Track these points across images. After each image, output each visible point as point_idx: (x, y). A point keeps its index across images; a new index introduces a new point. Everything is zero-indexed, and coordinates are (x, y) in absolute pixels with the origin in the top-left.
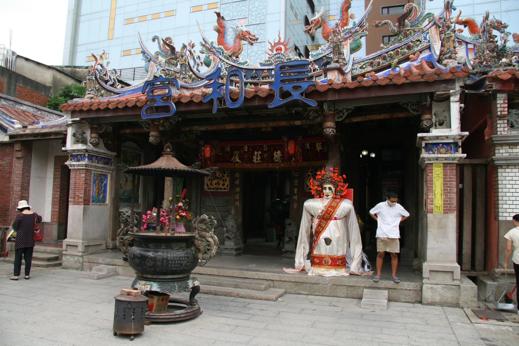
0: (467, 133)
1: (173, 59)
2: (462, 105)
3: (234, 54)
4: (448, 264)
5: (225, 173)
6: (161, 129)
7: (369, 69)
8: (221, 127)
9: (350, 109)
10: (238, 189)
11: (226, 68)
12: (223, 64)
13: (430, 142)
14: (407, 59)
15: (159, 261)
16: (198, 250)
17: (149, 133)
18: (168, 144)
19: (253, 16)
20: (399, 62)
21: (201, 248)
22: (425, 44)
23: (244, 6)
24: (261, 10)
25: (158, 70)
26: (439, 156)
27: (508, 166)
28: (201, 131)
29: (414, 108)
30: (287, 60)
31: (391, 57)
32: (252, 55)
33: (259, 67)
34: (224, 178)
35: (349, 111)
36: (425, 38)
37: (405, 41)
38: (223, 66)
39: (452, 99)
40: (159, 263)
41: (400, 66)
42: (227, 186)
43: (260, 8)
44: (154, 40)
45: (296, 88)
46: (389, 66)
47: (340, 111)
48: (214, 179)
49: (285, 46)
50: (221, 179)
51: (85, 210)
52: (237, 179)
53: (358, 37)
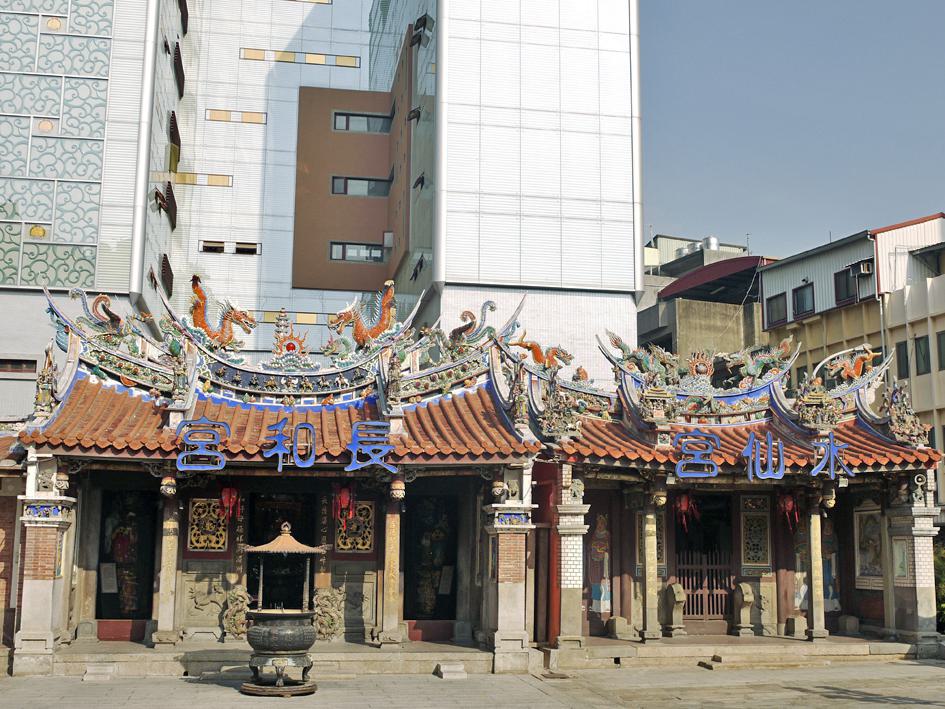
0: (536, 506)
1: (115, 335)
2: (535, 483)
4: (517, 632)
5: (220, 525)
7: (415, 391)
11: (209, 365)
12: (203, 356)
14: (462, 383)
17: (161, 479)
19: (72, 117)
22: (484, 368)
23: (50, 89)
24: (92, 109)
25: (85, 349)
26: (512, 526)
36: (484, 360)
38: (205, 362)
39: (525, 471)
42: (224, 544)
45: (374, 451)
46: (440, 391)
52: (240, 534)
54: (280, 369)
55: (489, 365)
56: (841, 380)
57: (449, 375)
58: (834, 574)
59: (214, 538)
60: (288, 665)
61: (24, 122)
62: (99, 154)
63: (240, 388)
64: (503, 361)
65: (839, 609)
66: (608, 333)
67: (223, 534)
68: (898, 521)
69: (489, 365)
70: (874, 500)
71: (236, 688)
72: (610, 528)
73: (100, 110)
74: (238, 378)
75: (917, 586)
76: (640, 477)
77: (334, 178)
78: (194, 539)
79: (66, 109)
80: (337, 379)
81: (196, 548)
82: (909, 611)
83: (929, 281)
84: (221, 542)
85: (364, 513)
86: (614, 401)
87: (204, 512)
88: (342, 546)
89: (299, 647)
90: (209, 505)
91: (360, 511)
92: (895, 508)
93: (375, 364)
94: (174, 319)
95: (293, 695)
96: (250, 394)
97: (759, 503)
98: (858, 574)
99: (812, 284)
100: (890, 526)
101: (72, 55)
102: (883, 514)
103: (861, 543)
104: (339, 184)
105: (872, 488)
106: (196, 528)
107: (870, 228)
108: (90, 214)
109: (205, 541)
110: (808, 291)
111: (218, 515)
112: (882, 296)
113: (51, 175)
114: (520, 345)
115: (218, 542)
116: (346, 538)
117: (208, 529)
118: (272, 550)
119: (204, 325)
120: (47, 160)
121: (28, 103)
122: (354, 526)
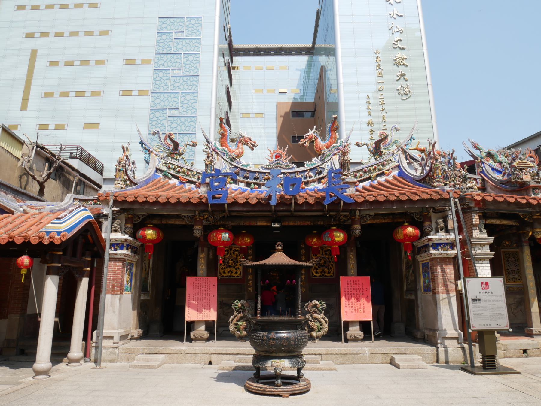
6: (205, 223)
8: (253, 223)
9: (145, 215)
10: (251, 277)
13: (435, 242)
14: (383, 174)
15: (293, 340)
16: (311, 329)
18: (279, 243)
20: (378, 175)
21: (315, 327)
22: (395, 164)
29: (418, 216)
30: (286, 166)
33: (261, 170)
34: (237, 267)
35: (144, 217)
36: (395, 159)
41: (378, 178)
43: (192, 101)
46: (369, 178)
47: (364, 217)
48: (227, 268)
50: (234, 268)
51: (120, 300)
55: (398, 162)
57: (375, 169)
59: (234, 270)
60: (286, 366)
61: (165, 111)
62: (195, 122)
63: (248, 180)
64: (407, 159)
66: (469, 140)
67: (240, 267)
69: (398, 162)
71: (239, 384)
73: (195, 104)
74: (246, 175)
78: (222, 271)
79: (181, 105)
80: (306, 173)
81: (223, 276)
84: (239, 273)
85: (328, 253)
87: (228, 254)
88: (315, 274)
89: (292, 352)
90: (231, 249)
91: (325, 251)
93: (329, 164)
94: (209, 143)
95: (291, 395)
96: (255, 184)
101: (183, 83)
106: (223, 264)
109: (228, 272)
111: (237, 256)
114: (417, 149)
115: (236, 273)
116: (317, 269)
117: (230, 264)
118: (267, 263)
120: (174, 125)
121: (166, 104)
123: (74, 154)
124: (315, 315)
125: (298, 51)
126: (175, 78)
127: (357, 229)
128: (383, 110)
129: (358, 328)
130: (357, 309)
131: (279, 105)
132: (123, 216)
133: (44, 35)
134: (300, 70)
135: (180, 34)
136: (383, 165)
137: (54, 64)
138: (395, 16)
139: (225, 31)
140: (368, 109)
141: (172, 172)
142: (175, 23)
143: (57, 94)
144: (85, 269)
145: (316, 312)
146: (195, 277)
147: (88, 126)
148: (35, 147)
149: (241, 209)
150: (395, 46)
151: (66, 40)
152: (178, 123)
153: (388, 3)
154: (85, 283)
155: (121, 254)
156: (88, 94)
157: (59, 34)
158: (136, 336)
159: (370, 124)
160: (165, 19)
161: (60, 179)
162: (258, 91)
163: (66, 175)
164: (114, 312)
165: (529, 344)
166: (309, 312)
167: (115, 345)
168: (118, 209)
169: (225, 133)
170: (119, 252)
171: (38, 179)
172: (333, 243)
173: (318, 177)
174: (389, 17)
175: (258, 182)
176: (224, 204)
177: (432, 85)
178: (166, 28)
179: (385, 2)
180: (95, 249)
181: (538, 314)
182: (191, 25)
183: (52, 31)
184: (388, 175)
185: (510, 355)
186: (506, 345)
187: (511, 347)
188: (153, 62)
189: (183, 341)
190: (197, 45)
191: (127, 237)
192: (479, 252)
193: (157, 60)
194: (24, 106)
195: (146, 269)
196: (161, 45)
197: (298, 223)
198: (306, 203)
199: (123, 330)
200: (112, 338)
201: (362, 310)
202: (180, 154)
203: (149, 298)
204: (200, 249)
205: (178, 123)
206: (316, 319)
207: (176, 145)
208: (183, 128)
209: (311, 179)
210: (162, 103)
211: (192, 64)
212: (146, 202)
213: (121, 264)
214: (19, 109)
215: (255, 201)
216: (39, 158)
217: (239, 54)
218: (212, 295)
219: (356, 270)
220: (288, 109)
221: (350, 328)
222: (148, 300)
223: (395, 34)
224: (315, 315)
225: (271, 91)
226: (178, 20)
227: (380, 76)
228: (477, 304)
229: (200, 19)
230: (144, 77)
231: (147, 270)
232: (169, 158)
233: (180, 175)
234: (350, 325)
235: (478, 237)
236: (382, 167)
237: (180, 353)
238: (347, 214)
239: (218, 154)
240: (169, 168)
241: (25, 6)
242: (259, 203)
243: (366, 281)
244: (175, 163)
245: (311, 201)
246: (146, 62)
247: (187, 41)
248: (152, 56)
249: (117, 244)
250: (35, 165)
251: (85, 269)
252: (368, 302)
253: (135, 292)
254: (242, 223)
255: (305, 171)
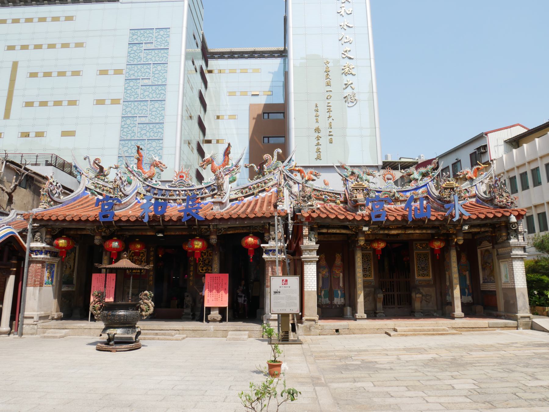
3: (149, 177)
6: (103, 234)
8: (144, 233)
14: (264, 190)
16: (142, 310)
20: (260, 192)
21: (144, 309)
22: (275, 182)
27: (309, 261)
28: (129, 235)
31: (254, 188)
32: (128, 88)
36: (275, 178)
37: (262, 179)
40: (122, 318)
41: (260, 194)
44: (85, 159)
46: (253, 194)
49: (186, 174)
51: (40, 290)
53: (234, 173)
54: (175, 187)
56: (466, 180)
57: (258, 187)
58: (468, 282)
63: (157, 197)
65: (472, 301)
68: (501, 251)
70: (488, 241)
72: (343, 260)
73: (162, 112)
74: (156, 192)
75: (516, 287)
76: (351, 230)
77: (264, 137)
79: (150, 112)
82: (512, 302)
83: (514, 151)
86: (343, 196)
92: (500, 243)
97: (424, 246)
98: (481, 282)
99: (460, 161)
100: (498, 254)
102: (493, 248)
103: (482, 265)
104: (266, 140)
105: (486, 234)
107: (484, 131)
108: (159, 151)
110: (459, 164)
112: (492, 161)
113: (145, 138)
119: (141, 169)
120: (143, 132)
122: (207, 261)
123: (49, 162)
124: (146, 301)
125: (271, 54)
126: (144, 87)
127: (214, 239)
128: (329, 117)
129: (217, 312)
130: (216, 298)
131: (252, 106)
132: (44, 230)
133: (24, 47)
134: (272, 73)
135: (149, 45)
136: (265, 183)
137: (33, 75)
138: (345, 27)
139: (195, 39)
140: (316, 116)
141: (98, 190)
142: (145, 35)
143: (36, 104)
144: (12, 269)
145: (146, 299)
146: (99, 274)
147: (65, 134)
148: (5, 162)
149: (125, 224)
150: (344, 56)
151: (45, 53)
152: (147, 130)
153: (339, 14)
154: (12, 279)
155: (40, 258)
156: (65, 103)
157: (38, 47)
158: (56, 317)
159: (317, 130)
160: (136, 31)
161: (30, 188)
162: (232, 94)
163: (37, 183)
164: (35, 300)
165: (341, 325)
166: (141, 299)
167: (35, 323)
168: (38, 225)
169: (140, 158)
170: (39, 256)
171: (6, 190)
172: (194, 250)
173: (211, 193)
174: (340, 28)
175: (164, 198)
176: (112, 222)
177: (378, 93)
178: (137, 39)
179: (336, 14)
180: (20, 254)
181: (363, 303)
182: (160, 36)
183: (32, 43)
184: (268, 192)
185: (325, 333)
186: (323, 326)
187: (327, 327)
188: (124, 72)
189: (88, 320)
190: (165, 55)
191: (44, 245)
192: (308, 256)
193: (128, 71)
194: (7, 115)
195: (70, 268)
196: (132, 55)
197: (177, 233)
198: (171, 220)
199: (43, 313)
200: (32, 318)
201: (220, 299)
202: (105, 176)
203: (74, 290)
204: (104, 253)
205: (147, 130)
206: (146, 303)
207: (101, 168)
208: (152, 134)
209: (206, 195)
210: (133, 111)
211: (133, 90)
212: (57, 220)
213: (41, 265)
214: (3, 118)
215: (134, 219)
216: (9, 171)
217: (214, 58)
218: (111, 287)
219: (219, 269)
220: (260, 112)
221: (212, 312)
222: (73, 291)
223: (344, 44)
224: (146, 301)
225: (244, 94)
226: (148, 32)
227: (328, 85)
228: (277, 295)
229: (168, 30)
230: (116, 86)
231: (72, 268)
232: (96, 179)
233: (104, 193)
234: (211, 310)
235: (307, 244)
236: (264, 185)
237: (80, 328)
238: (207, 227)
239: (134, 175)
240: (96, 187)
241: (6, 20)
242: (137, 220)
243: (225, 277)
244: (101, 182)
245: (175, 219)
246: (118, 72)
247: (156, 51)
248: (123, 66)
249: (38, 251)
250: (5, 178)
251: (12, 269)
252: (226, 293)
253: (56, 285)
254: (136, 233)
255: (202, 188)
